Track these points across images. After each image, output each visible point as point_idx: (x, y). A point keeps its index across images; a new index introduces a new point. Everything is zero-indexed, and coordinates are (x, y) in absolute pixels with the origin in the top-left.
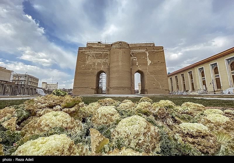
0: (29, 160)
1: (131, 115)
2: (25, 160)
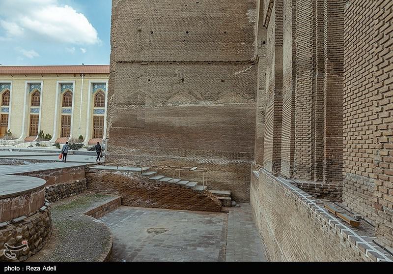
0: (48, 269)
1: (264, 40)
2: (42, 269)
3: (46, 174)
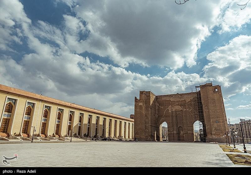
0: (31, 172)
2: (27, 171)
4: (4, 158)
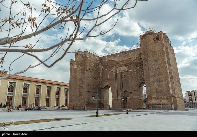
0: (24, 134)
2: (21, 134)
3: (131, 111)
4: (3, 123)
